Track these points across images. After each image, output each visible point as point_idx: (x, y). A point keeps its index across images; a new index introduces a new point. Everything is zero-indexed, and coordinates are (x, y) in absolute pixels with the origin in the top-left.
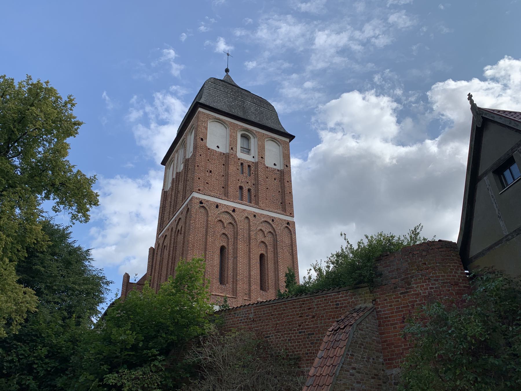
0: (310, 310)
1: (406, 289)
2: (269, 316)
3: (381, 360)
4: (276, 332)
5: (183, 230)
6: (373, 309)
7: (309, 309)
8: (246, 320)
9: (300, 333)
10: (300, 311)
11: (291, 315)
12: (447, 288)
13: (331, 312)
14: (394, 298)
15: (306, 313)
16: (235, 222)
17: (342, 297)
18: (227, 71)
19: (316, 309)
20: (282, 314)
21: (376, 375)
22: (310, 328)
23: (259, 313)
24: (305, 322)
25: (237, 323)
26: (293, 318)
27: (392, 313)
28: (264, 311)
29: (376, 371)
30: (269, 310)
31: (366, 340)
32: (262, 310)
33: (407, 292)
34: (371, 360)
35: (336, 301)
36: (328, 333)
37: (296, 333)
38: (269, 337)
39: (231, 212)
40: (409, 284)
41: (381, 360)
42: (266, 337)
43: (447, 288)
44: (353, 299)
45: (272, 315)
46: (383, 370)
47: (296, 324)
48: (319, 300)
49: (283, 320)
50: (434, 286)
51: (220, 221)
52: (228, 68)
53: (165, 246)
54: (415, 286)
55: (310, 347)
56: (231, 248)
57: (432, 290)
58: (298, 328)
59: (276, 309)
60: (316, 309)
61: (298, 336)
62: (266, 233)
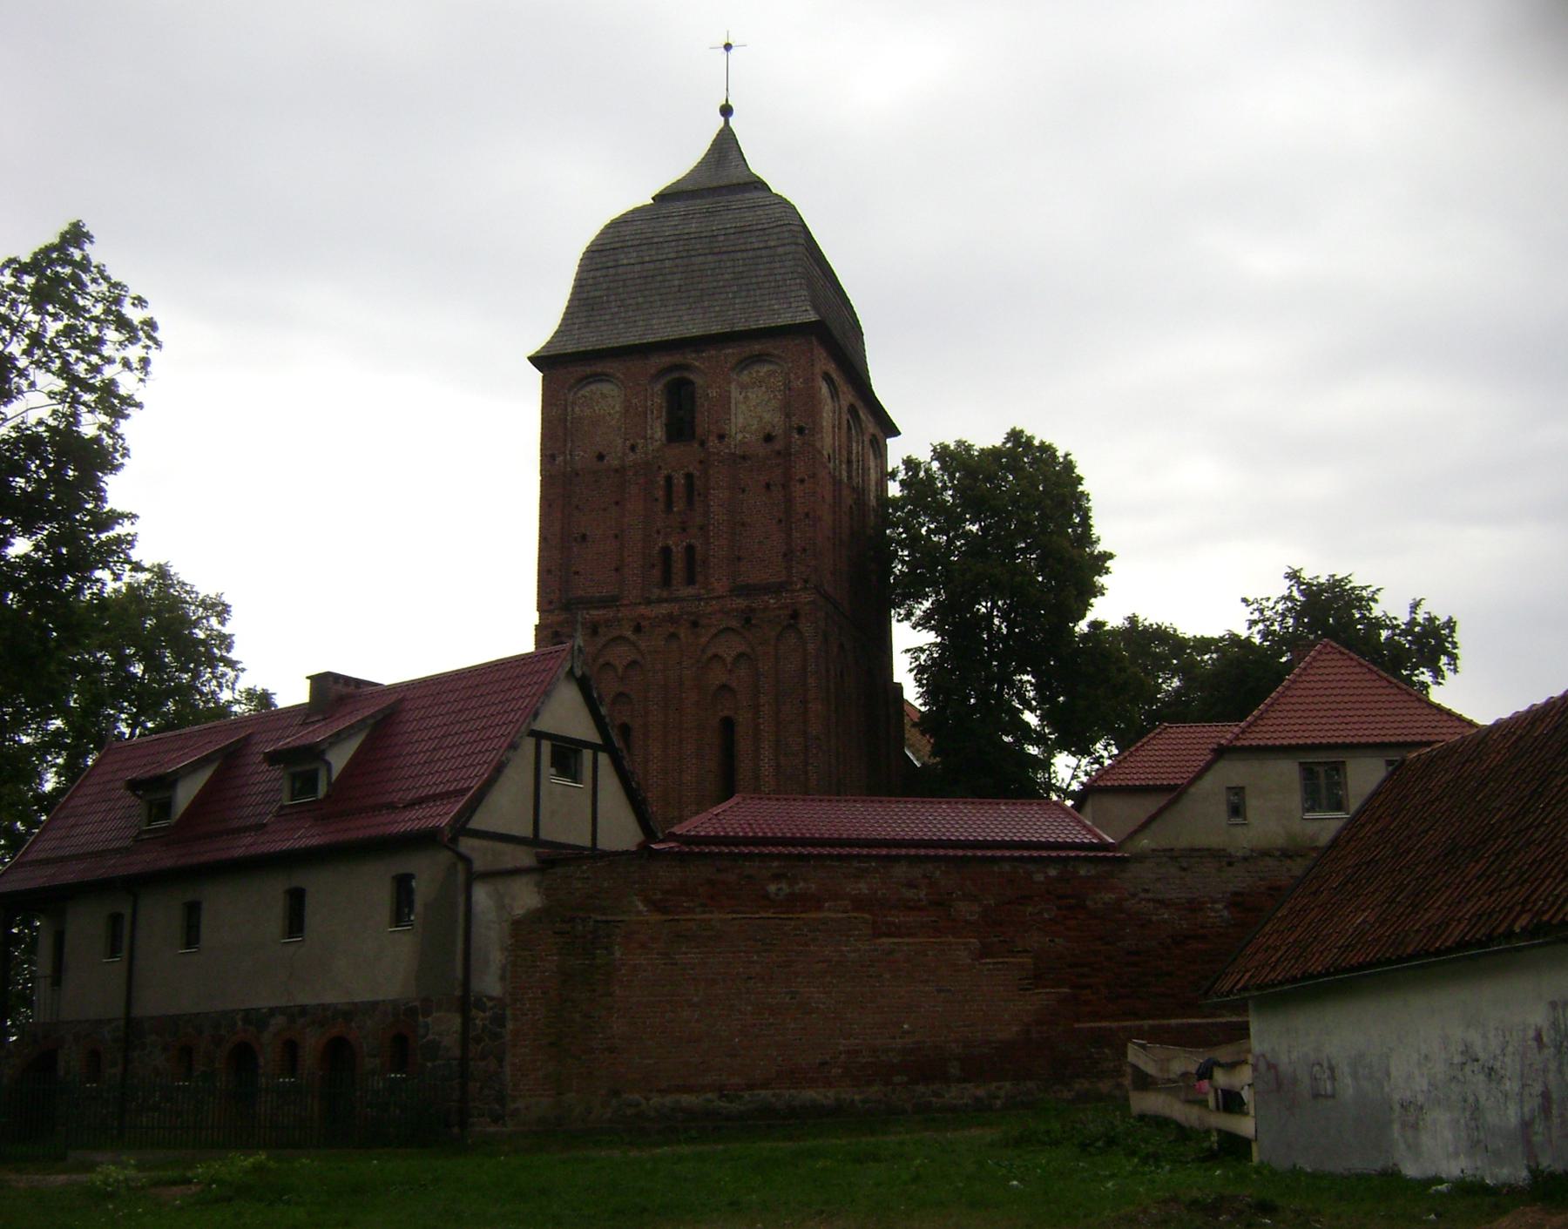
18: (726, 111)
39: (629, 634)
51: (608, 664)
52: (730, 103)
62: (729, 659)
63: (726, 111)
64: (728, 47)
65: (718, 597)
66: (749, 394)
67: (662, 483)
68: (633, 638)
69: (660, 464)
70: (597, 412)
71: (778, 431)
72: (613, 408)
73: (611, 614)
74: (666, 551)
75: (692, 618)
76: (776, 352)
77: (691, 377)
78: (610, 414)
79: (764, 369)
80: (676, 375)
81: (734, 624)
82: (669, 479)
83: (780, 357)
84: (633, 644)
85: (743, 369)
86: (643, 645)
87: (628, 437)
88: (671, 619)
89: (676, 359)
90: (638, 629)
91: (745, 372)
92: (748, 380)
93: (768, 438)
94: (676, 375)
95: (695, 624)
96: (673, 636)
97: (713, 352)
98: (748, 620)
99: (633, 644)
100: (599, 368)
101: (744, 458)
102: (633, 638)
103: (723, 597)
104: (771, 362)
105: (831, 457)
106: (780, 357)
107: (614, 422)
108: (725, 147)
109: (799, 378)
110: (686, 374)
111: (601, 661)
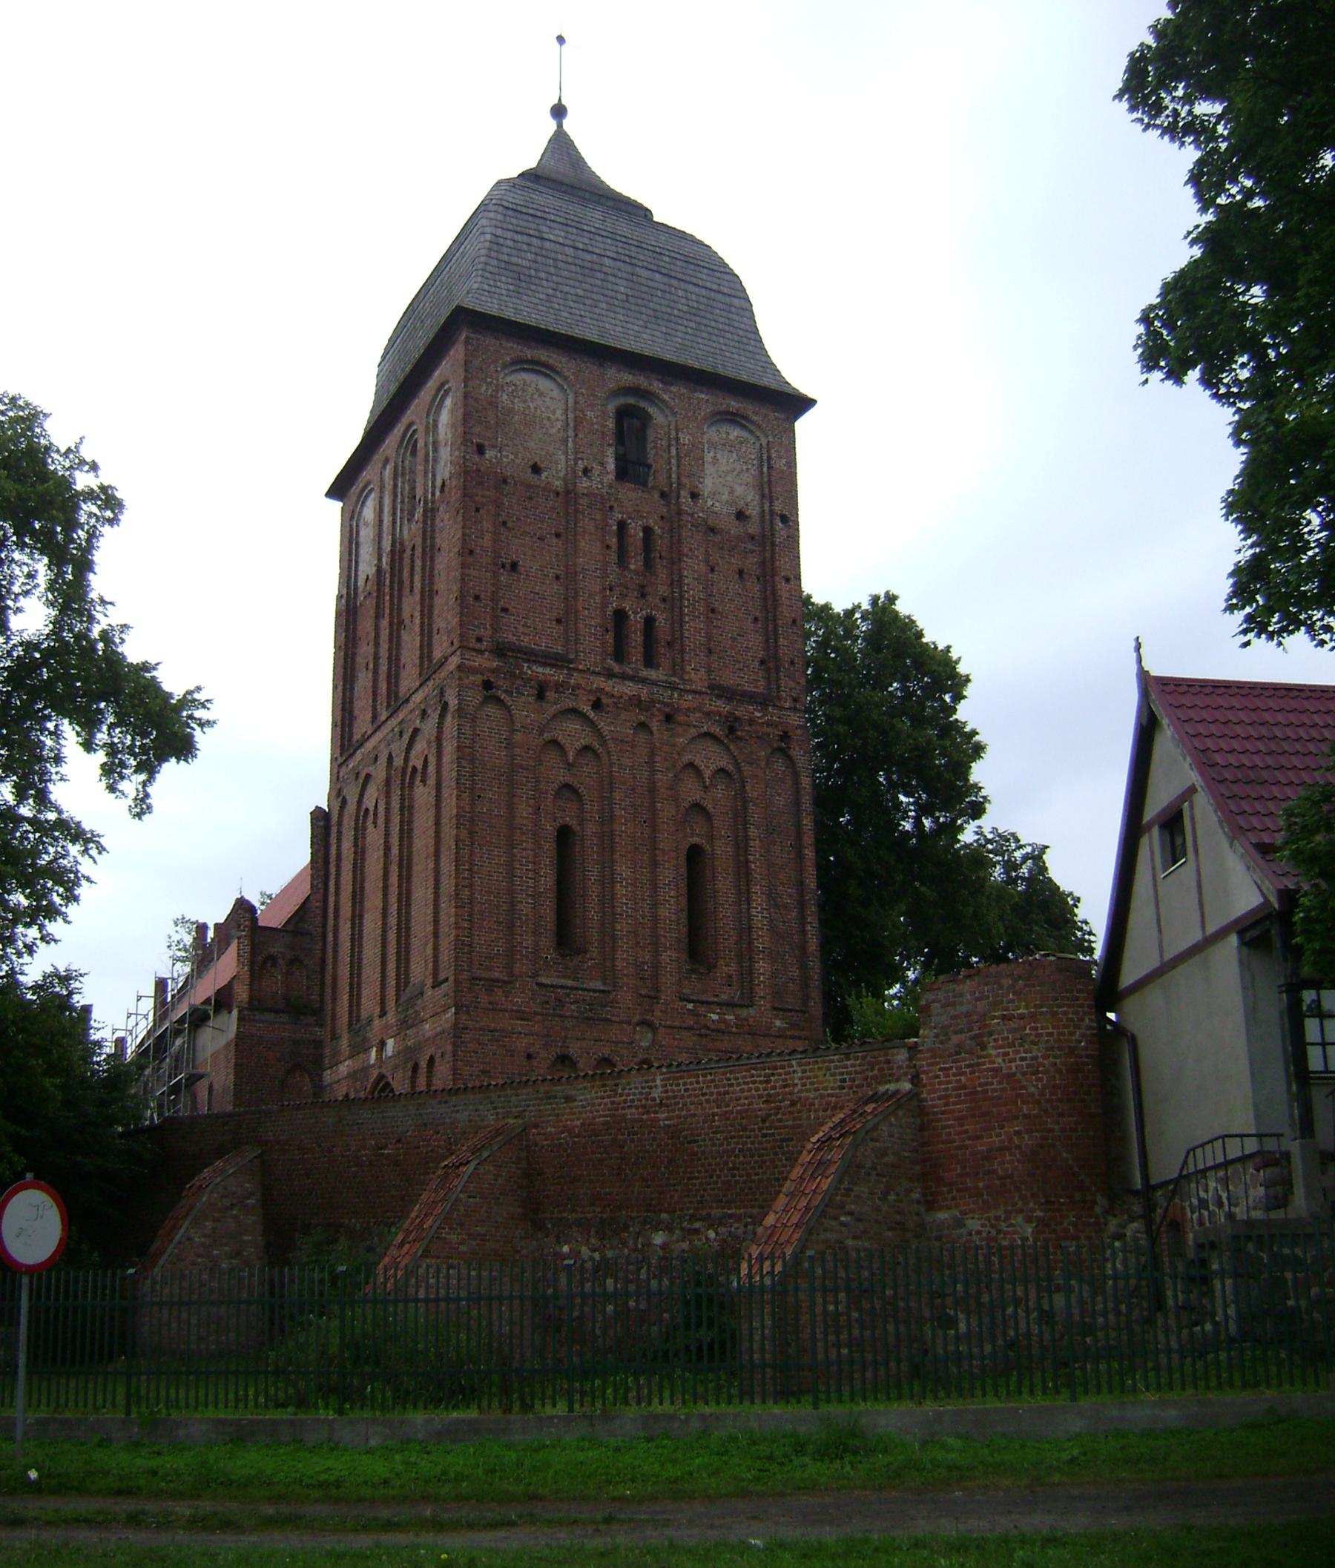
0: (787, 1089)
1: (979, 1057)
2: (695, 1096)
3: (916, 1196)
4: (713, 1133)
5: (432, 769)
6: (914, 1096)
7: (785, 1086)
8: (644, 1102)
9: (764, 1136)
10: (765, 1089)
11: (746, 1098)
12: (1051, 1060)
13: (829, 1095)
14: (954, 1075)
15: (778, 1094)
16: (604, 742)
17: (853, 1066)
18: (559, 111)
19: (799, 1087)
20: (727, 1093)
21: (898, 1223)
22: (786, 1127)
23: (674, 1087)
24: (776, 1114)
25: (623, 1108)
26: (751, 1103)
27: (947, 1104)
28: (685, 1084)
29: (898, 1217)
30: (698, 1082)
31: (886, 1160)
32: (681, 1081)
33: (979, 1064)
34: (892, 1197)
35: (842, 1074)
36: (809, 1146)
37: (756, 1136)
38: (697, 1141)
39: (586, 709)
40: (984, 1047)
41: (916, 1196)
42: (689, 1143)
43: (1051, 1060)
44: (876, 1072)
45: (704, 1094)
46: (918, 1214)
47: (756, 1117)
48: (807, 1068)
49: (729, 1106)
50: (1029, 1055)
51: (554, 742)
52: (564, 102)
53: (367, 810)
54: (993, 1052)
55: (785, 1166)
56: (591, 828)
57: (1024, 1063)
58: (760, 1125)
59: (713, 1081)
60: (799, 1087)
61: (760, 1143)
62: (707, 774)
63: (559, 111)
64: (561, 40)
65: (694, 692)
66: (719, 456)
67: (615, 528)
68: (592, 714)
69: (612, 503)
70: (532, 410)
71: (753, 511)
72: (554, 412)
73: (560, 677)
74: (620, 616)
75: (667, 710)
76: (756, 418)
77: (652, 410)
78: (549, 419)
79: (736, 433)
80: (631, 401)
81: (717, 730)
82: (622, 525)
83: (759, 427)
84: (591, 723)
85: (712, 424)
86: (606, 729)
87: (580, 456)
88: (636, 702)
89: (641, 381)
90: (597, 705)
91: (714, 429)
92: (717, 439)
93: (741, 516)
94: (631, 401)
95: (669, 718)
96: (643, 726)
97: (683, 391)
98: (732, 730)
99: (591, 723)
100: (542, 354)
101: (712, 530)
102: (592, 714)
103: (700, 693)
104: (744, 427)
105: (660, 543)
106: (759, 427)
107: (554, 431)
108: (561, 145)
109: (780, 458)
110: (643, 404)
111: (547, 736)
